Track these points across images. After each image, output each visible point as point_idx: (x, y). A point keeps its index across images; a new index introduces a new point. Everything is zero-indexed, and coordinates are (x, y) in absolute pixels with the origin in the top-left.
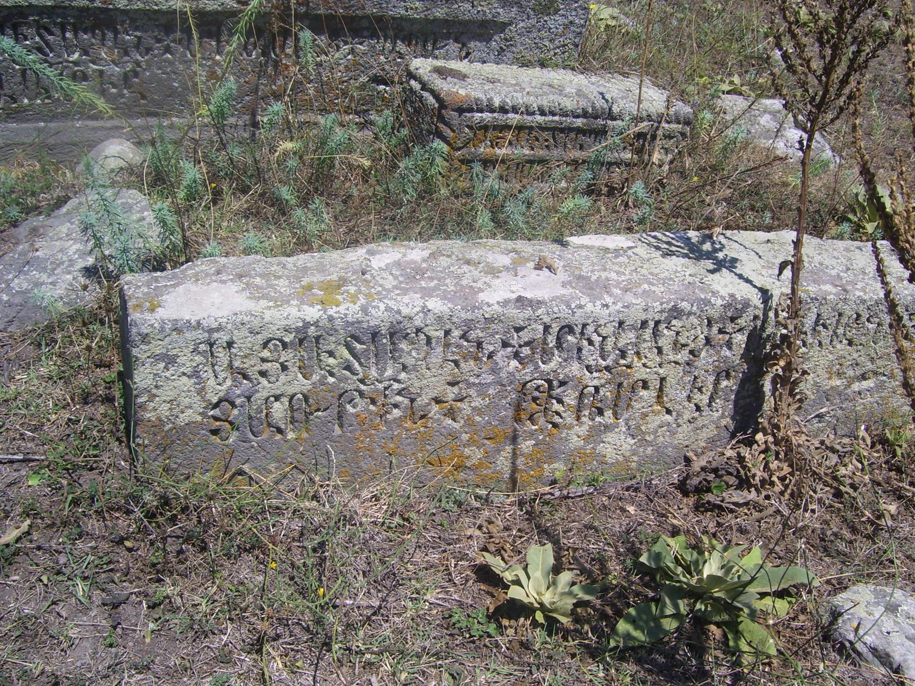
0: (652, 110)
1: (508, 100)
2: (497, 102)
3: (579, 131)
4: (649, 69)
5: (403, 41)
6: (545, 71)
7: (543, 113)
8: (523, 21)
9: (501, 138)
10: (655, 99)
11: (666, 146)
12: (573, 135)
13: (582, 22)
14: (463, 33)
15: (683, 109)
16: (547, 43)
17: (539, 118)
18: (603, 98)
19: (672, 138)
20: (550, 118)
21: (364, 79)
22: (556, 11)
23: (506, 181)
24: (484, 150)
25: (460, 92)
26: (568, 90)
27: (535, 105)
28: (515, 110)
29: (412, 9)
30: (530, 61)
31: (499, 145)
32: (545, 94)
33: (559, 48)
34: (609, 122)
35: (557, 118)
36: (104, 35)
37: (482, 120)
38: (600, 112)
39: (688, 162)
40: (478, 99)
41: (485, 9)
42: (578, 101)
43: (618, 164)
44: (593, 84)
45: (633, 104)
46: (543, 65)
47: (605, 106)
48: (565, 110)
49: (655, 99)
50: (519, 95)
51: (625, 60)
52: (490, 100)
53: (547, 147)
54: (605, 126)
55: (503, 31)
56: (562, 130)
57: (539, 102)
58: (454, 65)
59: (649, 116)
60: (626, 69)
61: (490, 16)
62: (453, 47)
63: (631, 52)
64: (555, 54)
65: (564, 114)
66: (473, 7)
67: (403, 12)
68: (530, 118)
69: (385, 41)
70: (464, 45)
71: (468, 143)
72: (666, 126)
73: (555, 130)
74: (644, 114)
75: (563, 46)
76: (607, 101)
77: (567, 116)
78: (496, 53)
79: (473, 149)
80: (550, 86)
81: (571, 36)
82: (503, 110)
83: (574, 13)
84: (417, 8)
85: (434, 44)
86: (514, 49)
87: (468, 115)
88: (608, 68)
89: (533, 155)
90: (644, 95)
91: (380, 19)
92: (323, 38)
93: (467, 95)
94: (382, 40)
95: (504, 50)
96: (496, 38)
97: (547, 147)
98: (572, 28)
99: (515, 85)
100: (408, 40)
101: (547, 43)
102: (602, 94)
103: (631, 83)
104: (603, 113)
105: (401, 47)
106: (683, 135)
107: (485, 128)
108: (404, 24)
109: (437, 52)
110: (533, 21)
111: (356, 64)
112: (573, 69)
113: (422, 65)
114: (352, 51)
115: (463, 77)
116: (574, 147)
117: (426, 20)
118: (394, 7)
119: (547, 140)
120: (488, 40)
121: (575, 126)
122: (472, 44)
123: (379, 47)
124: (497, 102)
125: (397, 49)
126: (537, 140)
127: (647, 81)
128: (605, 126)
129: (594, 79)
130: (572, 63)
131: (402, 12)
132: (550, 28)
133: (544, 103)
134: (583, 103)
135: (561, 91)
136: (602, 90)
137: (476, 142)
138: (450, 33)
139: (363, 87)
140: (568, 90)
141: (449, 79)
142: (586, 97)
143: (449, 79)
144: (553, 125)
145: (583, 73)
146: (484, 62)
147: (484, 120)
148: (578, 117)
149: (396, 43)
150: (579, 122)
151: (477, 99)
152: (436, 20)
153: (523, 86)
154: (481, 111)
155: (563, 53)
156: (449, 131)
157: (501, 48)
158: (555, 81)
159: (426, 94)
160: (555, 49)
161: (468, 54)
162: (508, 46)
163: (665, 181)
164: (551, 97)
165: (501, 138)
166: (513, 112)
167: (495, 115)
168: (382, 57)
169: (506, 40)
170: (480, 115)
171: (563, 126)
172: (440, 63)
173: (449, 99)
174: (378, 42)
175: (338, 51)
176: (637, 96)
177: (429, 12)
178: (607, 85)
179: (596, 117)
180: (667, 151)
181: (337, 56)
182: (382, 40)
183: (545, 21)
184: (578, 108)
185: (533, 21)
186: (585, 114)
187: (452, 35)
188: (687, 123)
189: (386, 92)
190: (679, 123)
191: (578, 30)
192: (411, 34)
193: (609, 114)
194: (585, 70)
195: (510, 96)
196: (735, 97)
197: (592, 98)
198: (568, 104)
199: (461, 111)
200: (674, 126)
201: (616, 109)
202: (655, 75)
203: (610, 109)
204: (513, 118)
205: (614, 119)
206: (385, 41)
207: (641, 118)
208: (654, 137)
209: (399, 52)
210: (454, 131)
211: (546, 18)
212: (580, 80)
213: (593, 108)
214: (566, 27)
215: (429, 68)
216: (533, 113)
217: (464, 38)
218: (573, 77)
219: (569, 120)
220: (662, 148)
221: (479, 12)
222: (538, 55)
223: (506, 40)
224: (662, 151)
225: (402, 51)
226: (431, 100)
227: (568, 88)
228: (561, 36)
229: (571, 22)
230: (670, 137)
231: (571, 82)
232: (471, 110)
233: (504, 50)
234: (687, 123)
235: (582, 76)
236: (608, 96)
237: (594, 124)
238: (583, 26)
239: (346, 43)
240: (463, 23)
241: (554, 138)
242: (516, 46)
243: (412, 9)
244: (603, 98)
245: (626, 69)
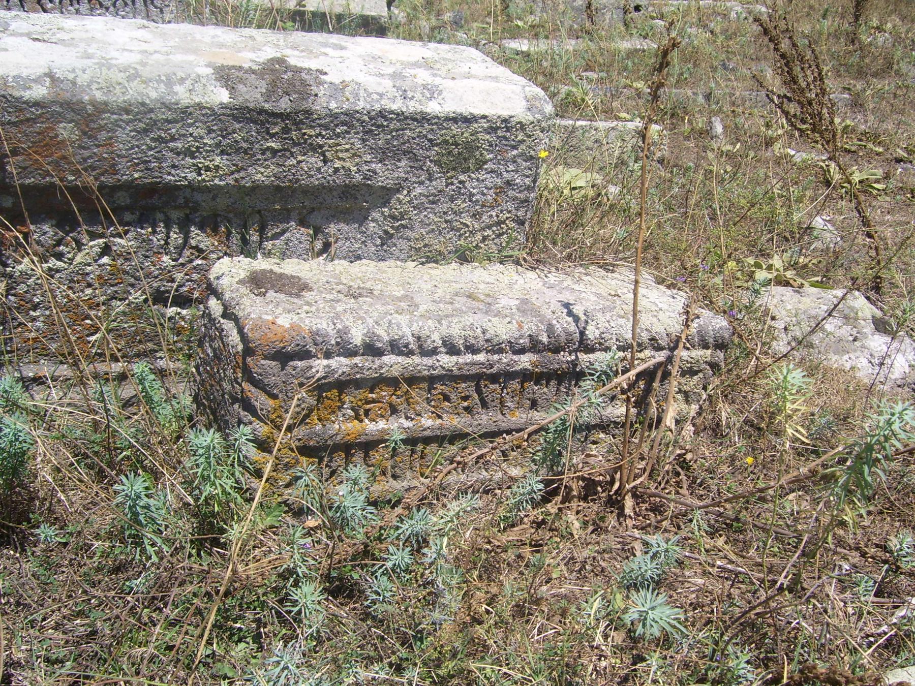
0: (659, 329)
1: (380, 331)
2: (357, 337)
3: (526, 376)
4: (648, 255)
5: (202, 228)
6: (466, 268)
7: (452, 350)
8: (421, 183)
9: (374, 401)
10: (664, 309)
11: (686, 388)
12: (515, 385)
13: (528, 181)
14: (313, 210)
15: (714, 323)
16: (468, 221)
17: (446, 360)
18: (570, 313)
19: (696, 373)
20: (469, 358)
21: (136, 296)
22: (480, 165)
23: (395, 477)
24: (343, 426)
25: (280, 321)
26: (504, 301)
27: (436, 337)
28: (396, 347)
29: (208, 169)
30: (440, 253)
31: (372, 416)
32: (460, 312)
33: (489, 227)
34: (582, 356)
35: (481, 357)
36: (229, 234)
37: (330, 372)
38: (563, 339)
39: (725, 411)
40: (317, 333)
41: (347, 164)
42: (520, 325)
43: (603, 426)
44: (551, 287)
45: (622, 321)
46: (464, 258)
47: (573, 328)
48: (495, 342)
49: (664, 309)
50: (403, 320)
51: (608, 246)
52: (343, 333)
53: (467, 409)
54: (574, 364)
55: (386, 203)
56: (494, 378)
57: (445, 331)
58: (291, 267)
59: (653, 339)
60: (609, 258)
61: (359, 177)
62: (298, 234)
63: (615, 231)
64: (485, 238)
65: (498, 349)
66: (325, 161)
67: (192, 176)
68: (428, 361)
69: (168, 228)
70: (317, 230)
71: (307, 416)
72: (684, 354)
73: (479, 379)
74: (645, 336)
75: (499, 223)
76: (577, 319)
77: (501, 351)
78: (379, 242)
79: (319, 427)
80: (469, 297)
81: (510, 206)
82: (372, 350)
83: (511, 168)
84: (217, 168)
85: (262, 231)
86: (410, 233)
87: (299, 364)
88: (580, 257)
89: (441, 427)
90: (643, 303)
91: (153, 190)
92: (46, 228)
93: (292, 327)
94: (161, 228)
95: (391, 236)
96: (376, 215)
97: (467, 409)
98: (511, 193)
99: (400, 299)
100: (210, 224)
101: (468, 221)
102: (567, 305)
103: (619, 281)
104: (569, 341)
105: (198, 238)
106: (714, 366)
107: (343, 385)
108: (198, 197)
109: (268, 245)
110: (440, 184)
111: (116, 272)
112: (517, 263)
113: (230, 270)
114: (106, 250)
115: (296, 287)
116: (519, 405)
117: (238, 187)
118: (174, 166)
119: (465, 398)
120: (362, 219)
121: (517, 368)
122: (332, 229)
123: (157, 240)
124: (357, 337)
125: (193, 243)
126: (447, 398)
127: (646, 276)
128: (574, 364)
129: (553, 278)
130: (516, 253)
131: (190, 176)
132: (472, 195)
133: (456, 330)
134: (531, 326)
135: (488, 305)
136: (568, 297)
137: (324, 413)
138: (288, 210)
139: (136, 311)
140: (504, 301)
141: (271, 294)
142: (536, 312)
143: (271, 294)
144: (475, 370)
145: (533, 269)
146: (359, 258)
147: (334, 371)
148: (522, 351)
149: (189, 232)
150: (525, 361)
151: (315, 334)
152: (256, 188)
153: (417, 300)
154: (328, 355)
155: (499, 236)
156: (263, 397)
157: (386, 232)
158: (482, 286)
159: (228, 326)
160: (483, 229)
161: (327, 246)
162: (397, 229)
163: (689, 456)
164: (469, 319)
165: (374, 401)
166: (392, 352)
167: (357, 360)
168: (165, 258)
169: (394, 218)
170: (325, 362)
171: (494, 370)
172: (261, 264)
173: (257, 335)
174: (154, 232)
175: (80, 250)
176: (629, 305)
177: (242, 174)
178: (576, 287)
179: (557, 350)
180: (687, 397)
181: (79, 259)
182: (161, 228)
183: (461, 182)
184: (521, 337)
185: (440, 184)
186: (535, 346)
187: (294, 214)
188: (721, 345)
189: (183, 318)
190: (706, 347)
191: (522, 196)
192: (216, 216)
193: (581, 342)
194: (536, 259)
195: (384, 323)
196: (780, 289)
197: (548, 314)
198: (502, 330)
199: (283, 357)
200: (698, 353)
201: (592, 333)
202: (655, 262)
203: (582, 333)
204: (393, 364)
205: (590, 350)
206: (168, 228)
207: (639, 345)
208: (666, 375)
209: (197, 248)
210: (274, 397)
211: (462, 178)
212: (528, 282)
213: (550, 329)
214: (500, 191)
215: (243, 275)
216: (434, 352)
217: (316, 219)
218: (516, 277)
219: (506, 358)
220: (680, 391)
221: (337, 170)
222: (450, 241)
223: (394, 218)
224: (679, 396)
225: (202, 246)
226: (234, 338)
227: (502, 300)
228: (493, 208)
229: (508, 183)
230: (692, 372)
231: (510, 286)
232: (305, 355)
233: (391, 236)
234: (721, 345)
235: (531, 275)
236: (578, 310)
237: (555, 364)
238: (529, 189)
239: (93, 236)
240: (308, 191)
241: (479, 391)
242: (412, 228)
243: (208, 169)
244: (570, 313)
245: (609, 258)
